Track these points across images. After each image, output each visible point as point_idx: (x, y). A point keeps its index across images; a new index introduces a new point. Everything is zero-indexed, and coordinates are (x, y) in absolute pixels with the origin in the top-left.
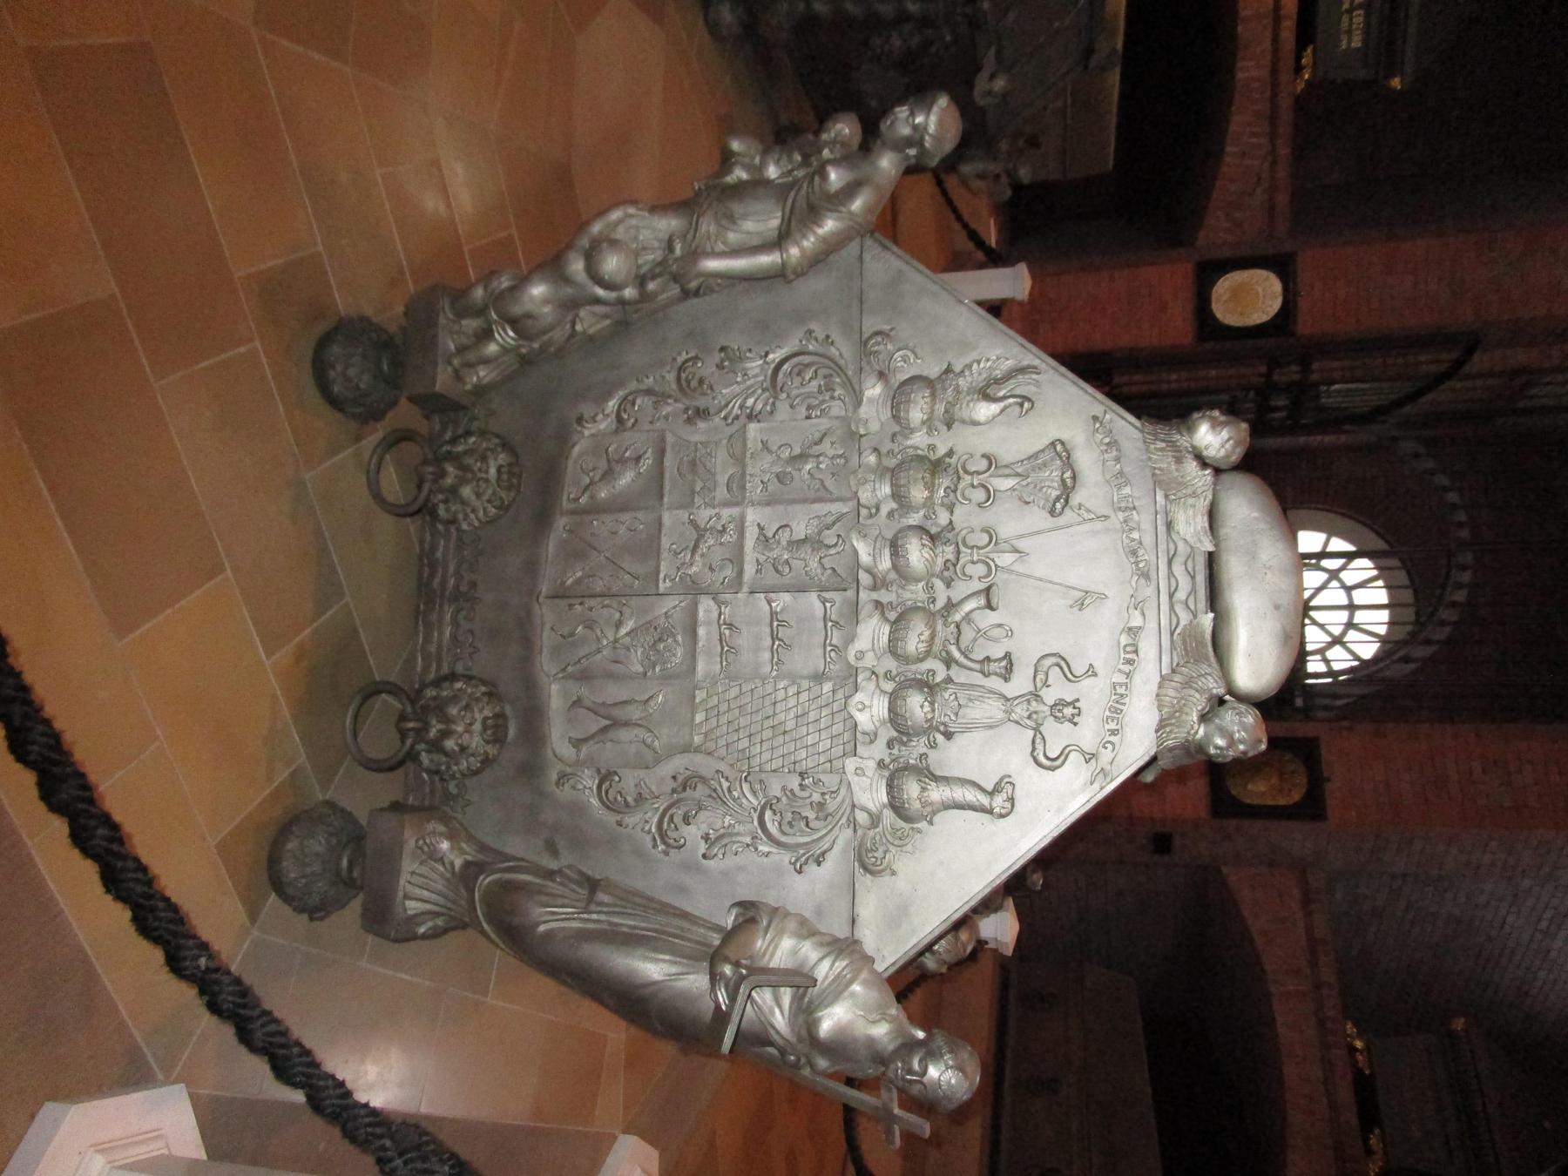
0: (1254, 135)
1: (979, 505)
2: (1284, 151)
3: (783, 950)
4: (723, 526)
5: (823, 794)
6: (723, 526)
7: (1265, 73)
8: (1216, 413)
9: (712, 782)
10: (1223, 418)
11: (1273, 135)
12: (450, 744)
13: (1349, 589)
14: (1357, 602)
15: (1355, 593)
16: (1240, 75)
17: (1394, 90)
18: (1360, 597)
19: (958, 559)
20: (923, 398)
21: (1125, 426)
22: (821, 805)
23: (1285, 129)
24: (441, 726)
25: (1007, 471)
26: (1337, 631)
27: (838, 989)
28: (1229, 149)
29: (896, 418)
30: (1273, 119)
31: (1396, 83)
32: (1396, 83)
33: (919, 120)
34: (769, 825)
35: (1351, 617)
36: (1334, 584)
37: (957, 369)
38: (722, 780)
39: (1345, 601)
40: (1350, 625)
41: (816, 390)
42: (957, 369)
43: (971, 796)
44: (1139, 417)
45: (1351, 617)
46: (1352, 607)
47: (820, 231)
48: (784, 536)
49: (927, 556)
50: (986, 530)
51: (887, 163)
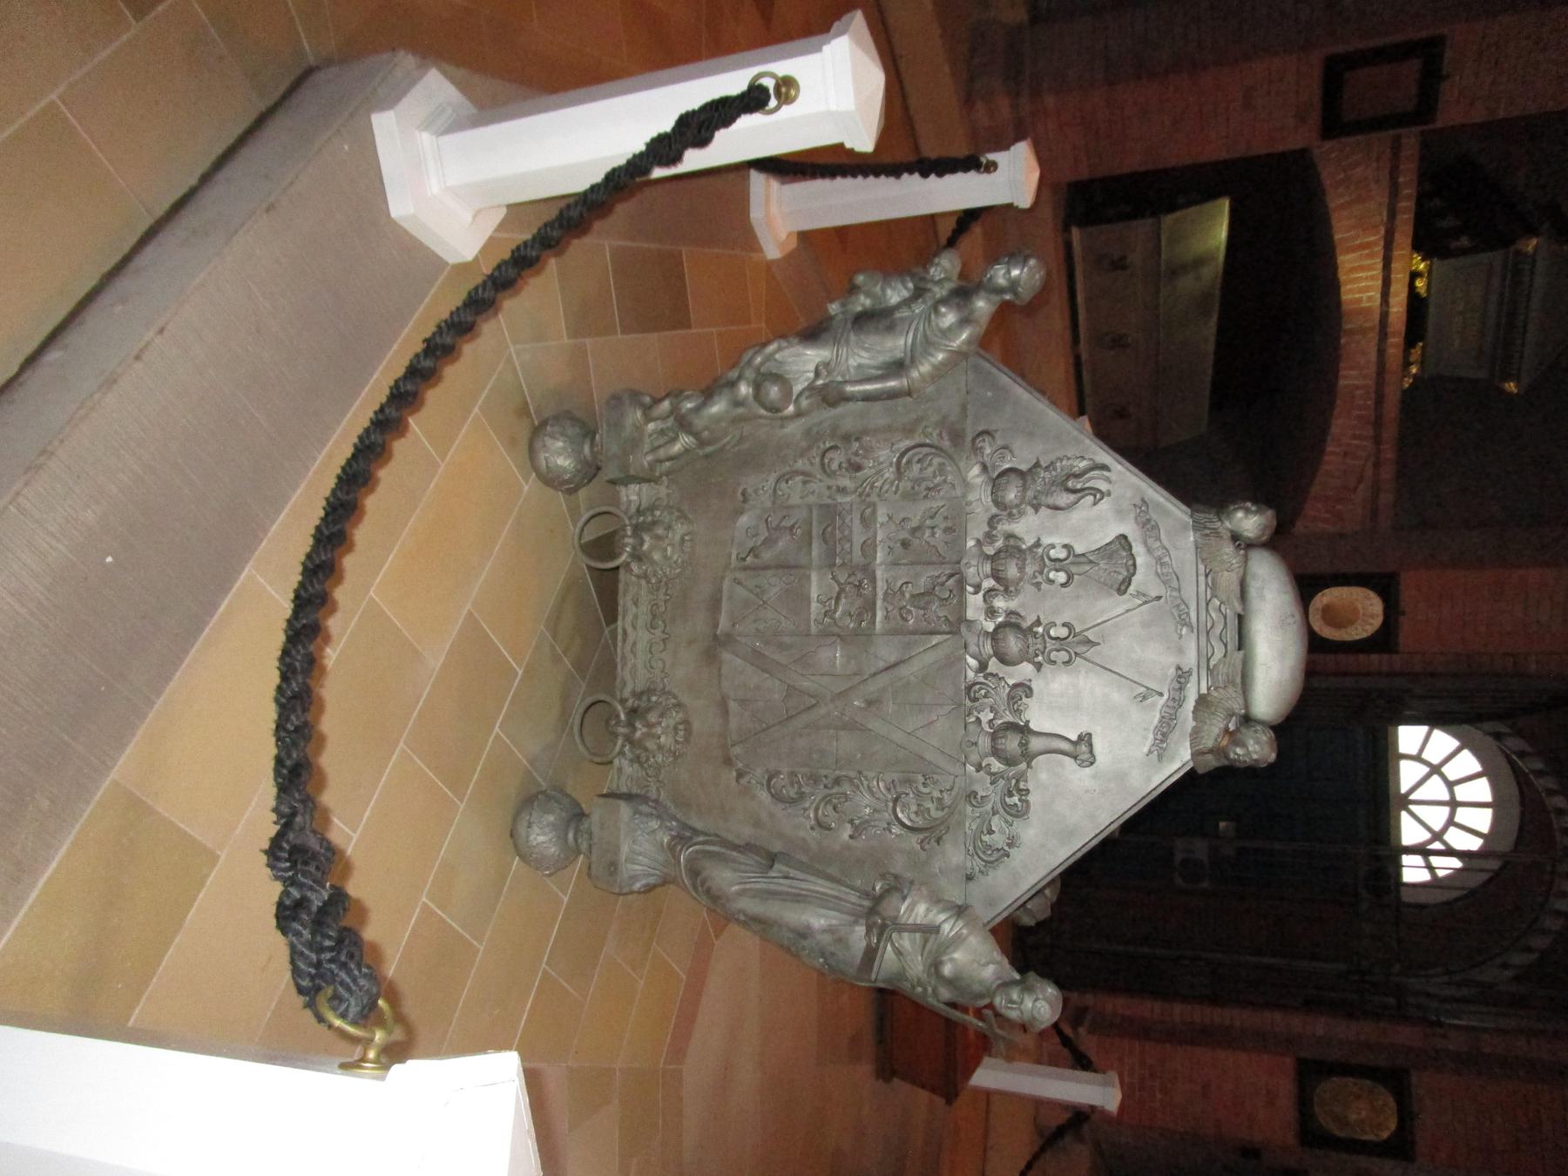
0: (1354, 437)
1: (1063, 585)
2: (1389, 454)
3: (919, 911)
4: (859, 582)
5: (941, 791)
6: (859, 582)
7: (1370, 382)
8: (1249, 504)
9: (855, 781)
10: (1254, 508)
11: (1377, 440)
12: (650, 745)
13: (1451, 785)
14: (1459, 798)
15: (1457, 789)
16: (1342, 383)
17: (1510, 394)
18: (1462, 793)
19: (1045, 648)
20: (1017, 487)
21: (1173, 511)
22: (940, 800)
23: (1390, 433)
24: (644, 730)
25: (1082, 559)
26: (1437, 827)
27: (957, 941)
28: (1329, 449)
29: (996, 503)
30: (1378, 422)
31: (1511, 387)
32: (1511, 387)
33: (965, 931)
34: (900, 815)
35: (1452, 814)
36: (1435, 778)
37: (1044, 464)
38: (862, 779)
39: (1446, 797)
40: (1451, 822)
41: (932, 475)
42: (1044, 464)
43: (1065, 746)
44: (1188, 504)
45: (1452, 814)
46: (1454, 804)
47: (933, 360)
48: (909, 590)
49: (1020, 645)
50: (1065, 546)
51: (982, 305)
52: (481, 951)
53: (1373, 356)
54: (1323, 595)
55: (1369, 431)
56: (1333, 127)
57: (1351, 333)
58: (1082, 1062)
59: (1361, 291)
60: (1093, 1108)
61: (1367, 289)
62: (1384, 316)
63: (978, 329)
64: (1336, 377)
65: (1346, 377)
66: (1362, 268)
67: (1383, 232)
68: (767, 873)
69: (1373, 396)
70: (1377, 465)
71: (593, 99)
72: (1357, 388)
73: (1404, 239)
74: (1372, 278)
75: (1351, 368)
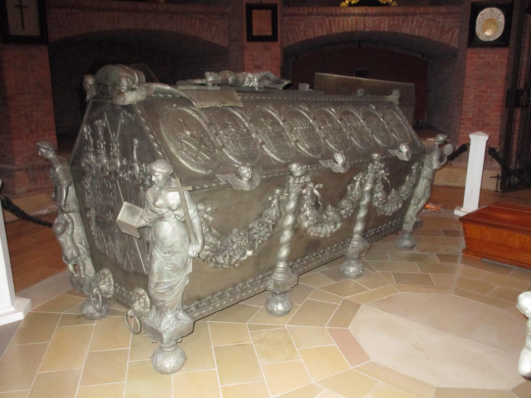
0: (412, 23)
7: (387, 18)
11: (414, 14)
52: (249, 331)
53: (376, 18)
54: (478, 34)
55: (410, 18)
56: (273, 38)
57: (365, 27)
58: (465, 148)
59: (348, 24)
60: (487, 146)
61: (347, 21)
62: (359, 15)
63: (436, 152)
64: (383, 32)
65: (384, 28)
66: (339, 24)
67: (325, 17)
68: (82, 254)
69: (394, 17)
70: (427, 14)
71: (5, 258)
72: (389, 23)
73: (333, 10)
74: (343, 20)
75: (380, 27)
